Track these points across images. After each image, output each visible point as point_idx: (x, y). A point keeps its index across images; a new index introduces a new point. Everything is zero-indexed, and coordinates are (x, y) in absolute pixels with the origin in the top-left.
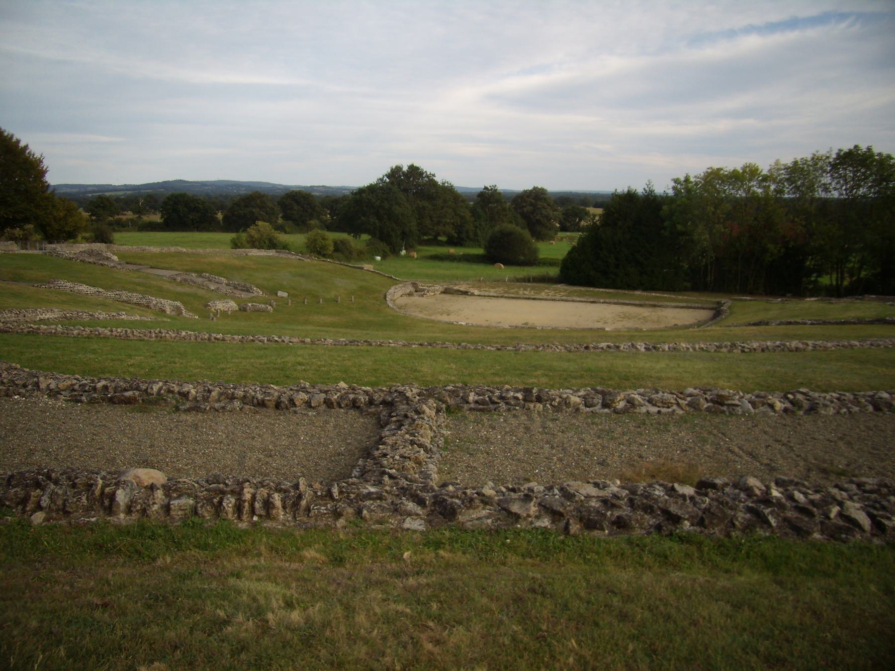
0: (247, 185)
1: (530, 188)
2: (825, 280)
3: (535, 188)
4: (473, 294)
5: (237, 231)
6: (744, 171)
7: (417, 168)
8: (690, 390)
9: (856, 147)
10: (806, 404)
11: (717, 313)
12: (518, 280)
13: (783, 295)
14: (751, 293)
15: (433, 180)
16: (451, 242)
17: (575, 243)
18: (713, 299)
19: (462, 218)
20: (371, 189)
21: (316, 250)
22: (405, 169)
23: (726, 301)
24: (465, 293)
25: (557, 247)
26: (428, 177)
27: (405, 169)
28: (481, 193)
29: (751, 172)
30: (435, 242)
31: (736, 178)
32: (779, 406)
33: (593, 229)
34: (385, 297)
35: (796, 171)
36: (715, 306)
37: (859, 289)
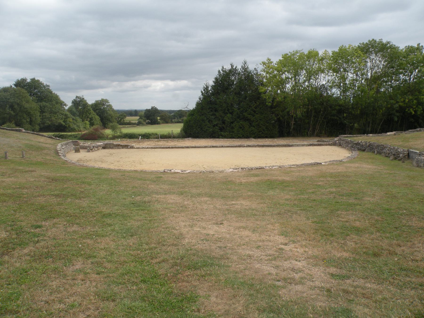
4: (132, 147)
26: (44, 87)
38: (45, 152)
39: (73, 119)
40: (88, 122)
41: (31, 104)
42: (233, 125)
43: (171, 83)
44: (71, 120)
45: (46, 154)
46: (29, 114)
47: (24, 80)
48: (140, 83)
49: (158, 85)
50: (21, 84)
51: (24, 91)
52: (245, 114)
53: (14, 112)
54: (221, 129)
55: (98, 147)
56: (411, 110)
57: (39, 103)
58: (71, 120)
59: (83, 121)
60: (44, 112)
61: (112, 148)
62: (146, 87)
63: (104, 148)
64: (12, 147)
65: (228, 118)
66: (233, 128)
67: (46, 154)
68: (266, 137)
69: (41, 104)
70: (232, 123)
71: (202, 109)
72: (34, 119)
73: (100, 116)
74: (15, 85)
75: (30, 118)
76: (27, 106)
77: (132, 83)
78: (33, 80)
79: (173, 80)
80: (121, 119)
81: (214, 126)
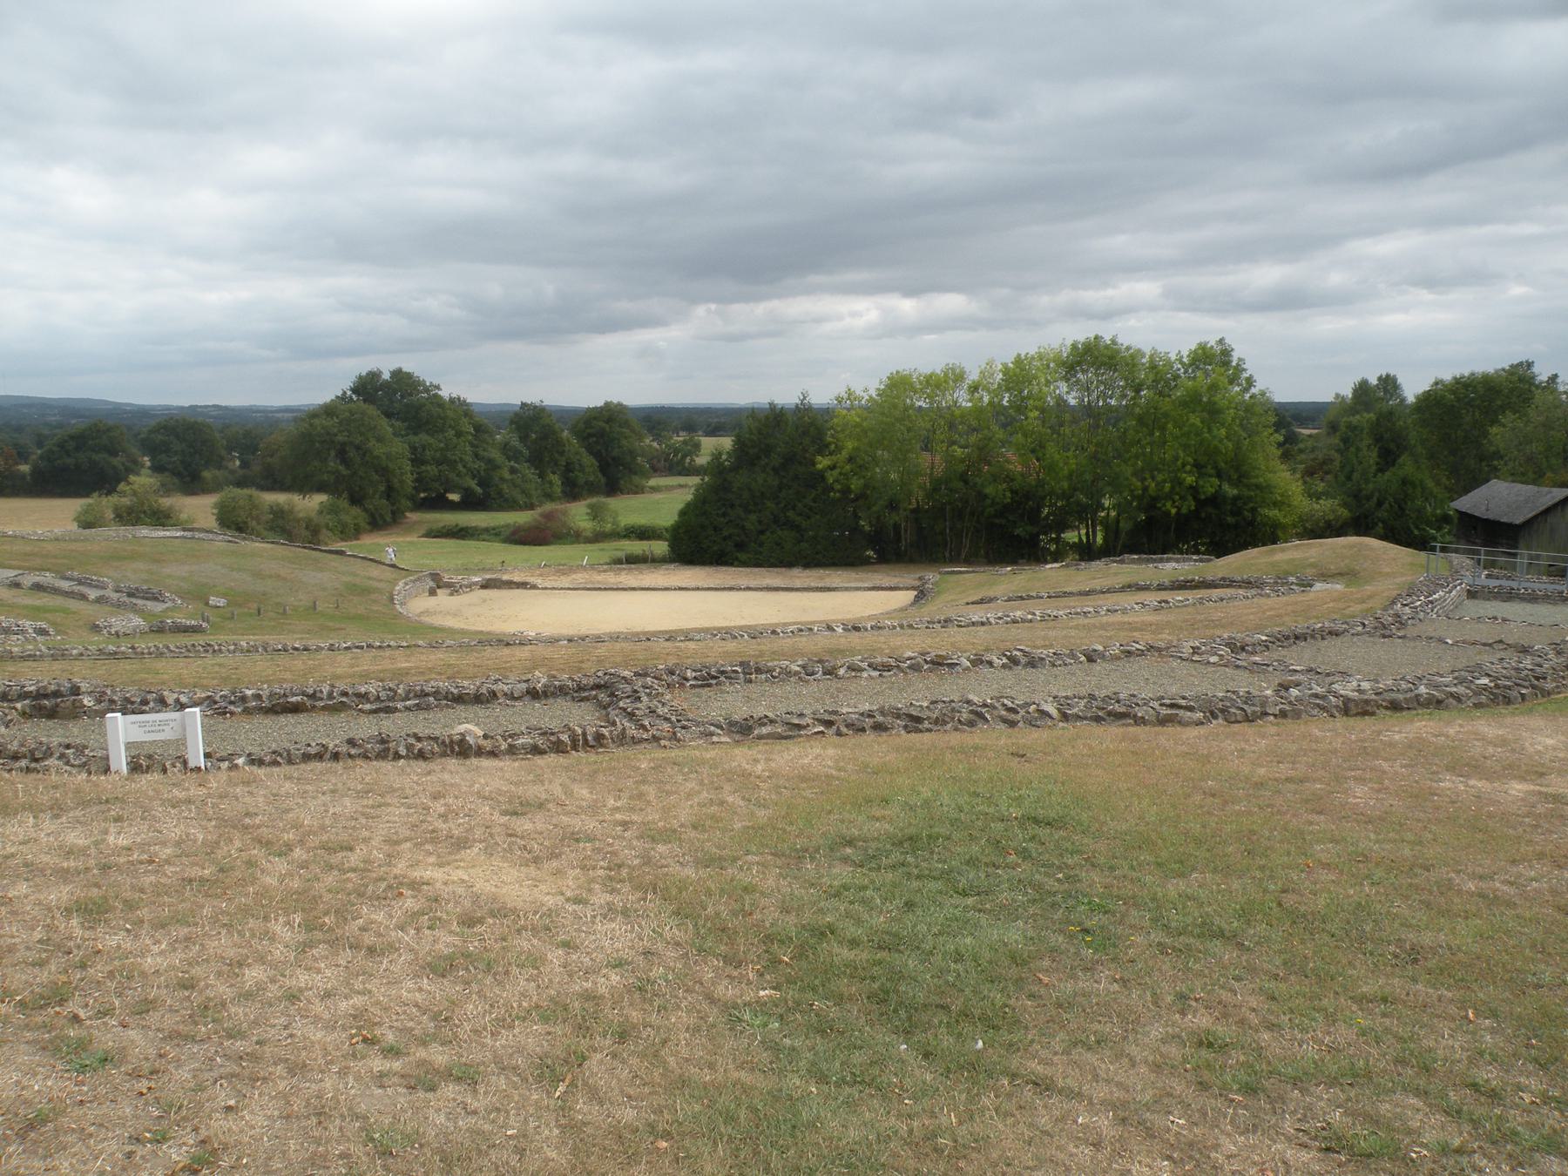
0: (68, 409)
1: (600, 403)
2: (1071, 536)
3: (607, 404)
4: (534, 587)
5: (87, 495)
6: (946, 374)
7: (409, 376)
8: (910, 654)
9: (1096, 338)
10: (1023, 660)
11: (922, 595)
12: (618, 561)
13: (1013, 562)
14: (968, 562)
15: (436, 395)
16: (471, 503)
17: (689, 497)
18: (909, 576)
19: (490, 461)
20: (328, 410)
21: (233, 522)
22: (386, 376)
23: (932, 576)
24: (523, 585)
25: (664, 502)
26: (427, 390)
27: (386, 376)
28: (516, 414)
29: (955, 376)
30: (438, 503)
31: (935, 384)
32: (997, 662)
33: (717, 468)
34: (392, 599)
35: (1018, 376)
36: (917, 583)
37: (1109, 551)
38: (373, 596)
39: (513, 471)
40: (556, 479)
41: (392, 446)
42: (763, 538)
43: (907, 307)
44: (507, 476)
45: (374, 601)
46: (384, 472)
47: (374, 375)
48: (796, 307)
49: (864, 311)
50: (368, 387)
51: (372, 410)
52: (790, 514)
53: (348, 466)
54: (740, 546)
55: (470, 586)
56: (1169, 504)
57: (412, 438)
58: (507, 476)
59: (541, 476)
60: (423, 462)
61: (499, 588)
62: (819, 320)
63: (484, 587)
64: (324, 589)
65: (751, 522)
66: (761, 545)
67: (374, 601)
68: (790, 565)
69: (416, 439)
70: (762, 532)
71: (704, 502)
72: (397, 485)
73: (597, 455)
74: (354, 390)
75: (388, 481)
76: (379, 450)
77: (774, 304)
78: (398, 374)
79: (910, 291)
80: (684, 457)
81: (725, 539)
